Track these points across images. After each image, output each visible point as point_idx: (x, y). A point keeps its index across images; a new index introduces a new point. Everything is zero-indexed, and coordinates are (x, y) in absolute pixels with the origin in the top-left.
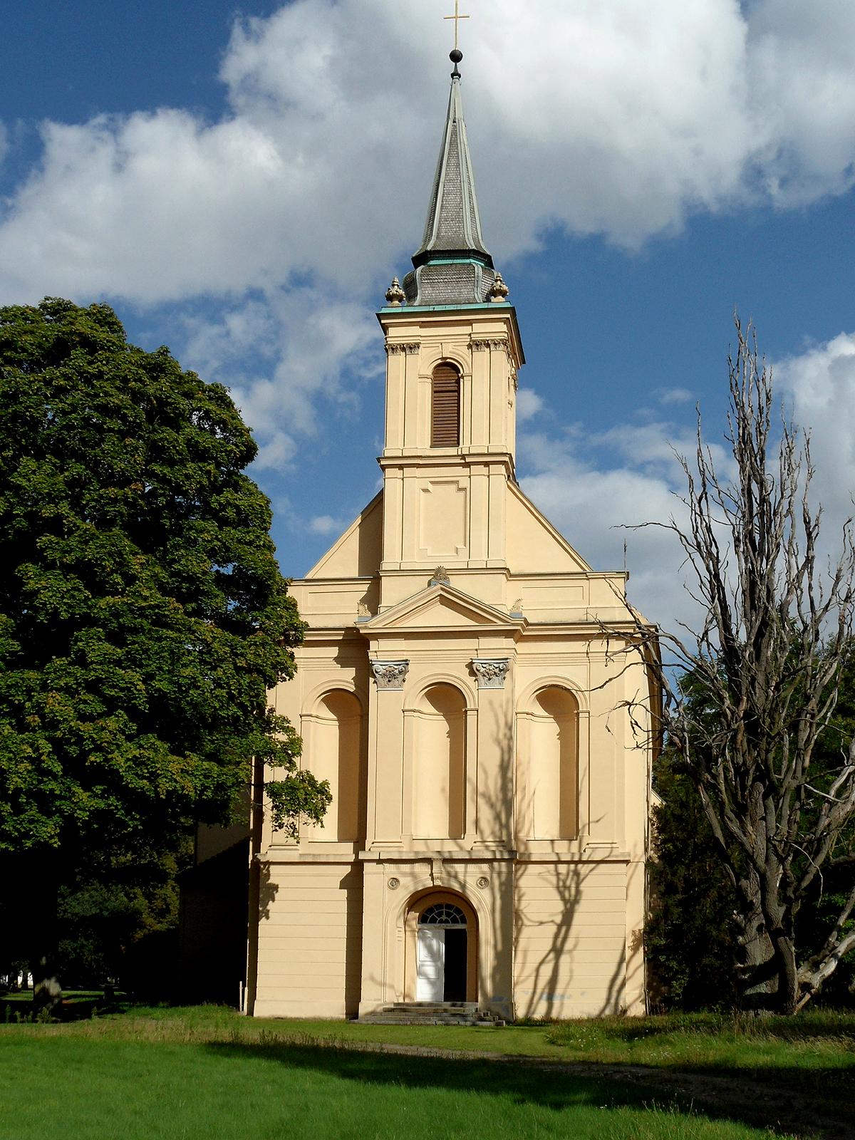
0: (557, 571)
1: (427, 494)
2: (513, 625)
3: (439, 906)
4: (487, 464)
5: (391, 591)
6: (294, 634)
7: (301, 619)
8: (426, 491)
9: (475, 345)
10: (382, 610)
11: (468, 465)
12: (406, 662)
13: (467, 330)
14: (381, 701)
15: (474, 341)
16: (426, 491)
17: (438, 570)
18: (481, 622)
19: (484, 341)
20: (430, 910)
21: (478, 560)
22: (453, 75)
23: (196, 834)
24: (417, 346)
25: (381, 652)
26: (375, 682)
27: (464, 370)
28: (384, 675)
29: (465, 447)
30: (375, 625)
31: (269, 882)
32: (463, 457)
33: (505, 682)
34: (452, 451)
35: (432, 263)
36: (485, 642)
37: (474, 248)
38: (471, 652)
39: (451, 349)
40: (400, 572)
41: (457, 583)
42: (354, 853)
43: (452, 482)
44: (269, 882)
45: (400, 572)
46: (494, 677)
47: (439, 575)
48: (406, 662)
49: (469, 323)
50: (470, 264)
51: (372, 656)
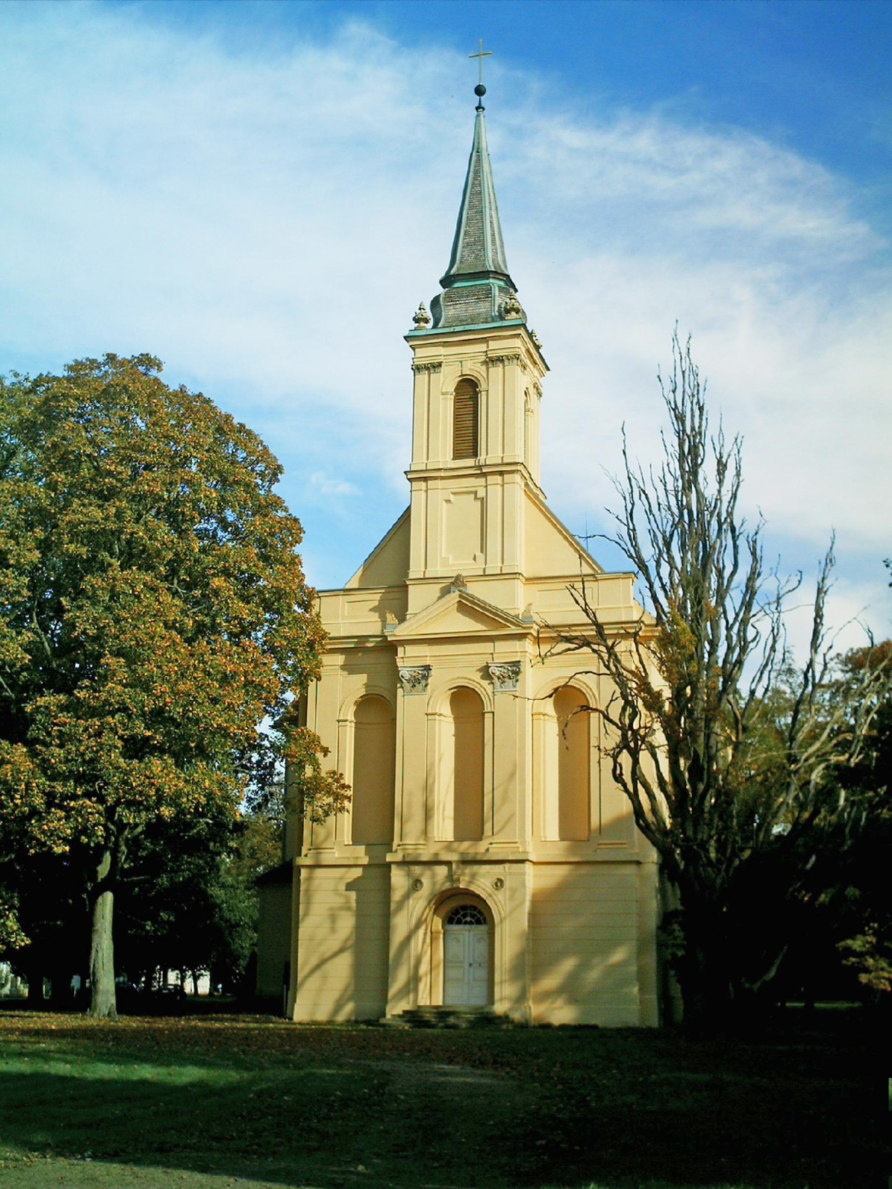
0: (332, 588)
1: (450, 505)
2: (525, 628)
3: (464, 908)
4: (501, 473)
5: (418, 597)
6: (316, 643)
7: (323, 627)
8: (448, 501)
9: (492, 361)
10: (408, 617)
11: (485, 475)
12: (427, 668)
13: (482, 347)
14: (408, 706)
15: (490, 358)
16: (448, 501)
17: (458, 577)
18: (495, 624)
19: (514, 355)
20: (456, 912)
21: (494, 567)
22: (477, 108)
23: (285, 839)
24: (440, 365)
25: (408, 660)
26: (402, 687)
27: (483, 386)
28: (408, 681)
29: (482, 458)
30: (402, 632)
31: (680, 908)
32: (480, 467)
33: (518, 683)
34: (470, 462)
35: (456, 285)
36: (501, 646)
37: (493, 269)
38: (486, 656)
39: (469, 366)
40: (425, 580)
41: (475, 589)
42: (366, 854)
43: (471, 492)
44: (680, 908)
45: (425, 580)
46: (507, 680)
47: (458, 582)
48: (427, 668)
49: (485, 340)
50: (488, 284)
51: (399, 663)
